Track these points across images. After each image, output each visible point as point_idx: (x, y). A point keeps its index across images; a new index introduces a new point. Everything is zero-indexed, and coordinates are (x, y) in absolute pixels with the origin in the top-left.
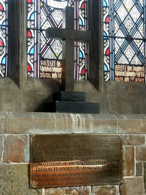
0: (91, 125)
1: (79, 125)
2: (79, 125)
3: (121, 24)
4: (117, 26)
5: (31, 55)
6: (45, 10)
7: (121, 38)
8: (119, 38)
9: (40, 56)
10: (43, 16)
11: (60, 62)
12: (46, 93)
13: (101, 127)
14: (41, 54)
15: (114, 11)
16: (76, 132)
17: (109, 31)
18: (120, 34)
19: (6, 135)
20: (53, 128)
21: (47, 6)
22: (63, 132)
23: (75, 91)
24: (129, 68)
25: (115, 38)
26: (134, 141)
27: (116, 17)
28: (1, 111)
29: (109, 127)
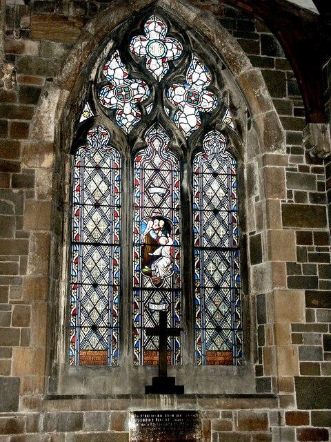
0: (176, 403)
1: (166, 404)
2: (166, 404)
3: (211, 318)
4: (207, 319)
5: (115, 303)
6: (148, 313)
7: (212, 329)
8: (209, 329)
9: (144, 349)
10: (146, 317)
11: (157, 376)
12: (46, 157)
13: (183, 405)
14: (144, 347)
15: (205, 308)
16: (164, 409)
17: (200, 324)
18: (210, 326)
19: (112, 411)
20: (146, 407)
21: (149, 309)
22: (295, 238)
23: (168, 376)
24: (219, 353)
25: (206, 329)
26: (211, 415)
27: (207, 312)
28: (271, 439)
29: (190, 405)
